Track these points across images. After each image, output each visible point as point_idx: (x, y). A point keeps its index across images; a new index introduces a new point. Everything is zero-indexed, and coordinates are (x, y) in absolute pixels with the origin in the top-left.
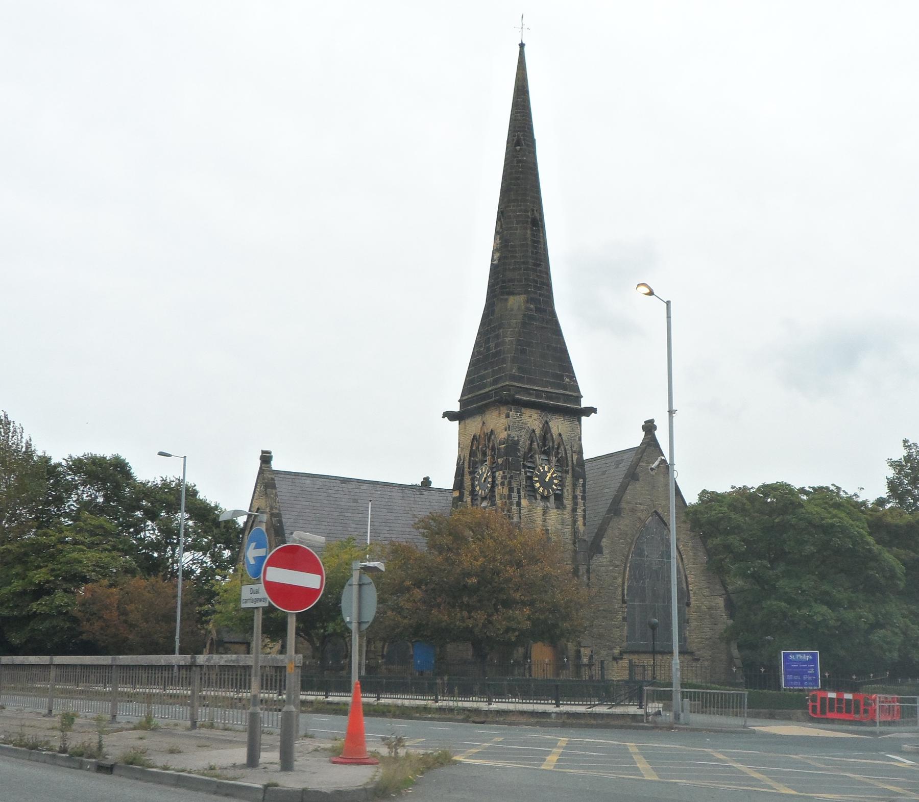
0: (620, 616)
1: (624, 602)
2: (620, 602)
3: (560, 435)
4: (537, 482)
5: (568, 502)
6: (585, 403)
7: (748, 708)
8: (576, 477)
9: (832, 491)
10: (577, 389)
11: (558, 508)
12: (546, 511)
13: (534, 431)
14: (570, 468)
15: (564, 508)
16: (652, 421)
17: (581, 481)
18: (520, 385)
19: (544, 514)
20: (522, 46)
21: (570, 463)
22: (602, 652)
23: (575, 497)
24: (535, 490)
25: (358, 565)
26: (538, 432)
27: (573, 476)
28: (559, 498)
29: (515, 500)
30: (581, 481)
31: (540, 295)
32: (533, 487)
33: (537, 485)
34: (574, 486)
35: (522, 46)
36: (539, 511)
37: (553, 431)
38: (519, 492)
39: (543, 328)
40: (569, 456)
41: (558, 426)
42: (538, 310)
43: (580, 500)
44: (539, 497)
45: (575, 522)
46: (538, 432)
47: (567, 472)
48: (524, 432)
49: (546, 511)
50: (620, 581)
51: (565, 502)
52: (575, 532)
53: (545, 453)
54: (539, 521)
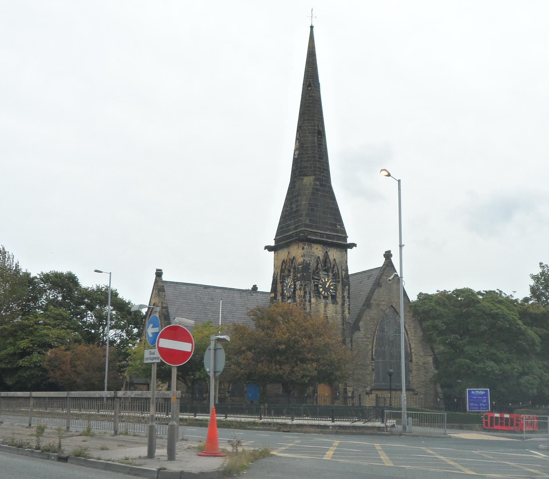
0: (370, 368)
1: (373, 359)
2: (371, 359)
3: (335, 260)
4: (321, 288)
5: (339, 300)
6: (349, 241)
7: (447, 423)
8: (344, 285)
10: (345, 232)
11: (333, 303)
12: (326, 305)
13: (319, 257)
14: (340, 279)
15: (337, 303)
16: (389, 252)
17: (347, 287)
18: (310, 230)
19: (325, 307)
20: (312, 27)
21: (340, 277)
22: (360, 389)
23: (343, 297)
24: (319, 293)
26: (321, 258)
27: (342, 284)
28: (334, 297)
29: (308, 299)
30: (347, 287)
31: (323, 176)
32: (318, 291)
33: (321, 290)
34: (343, 290)
35: (312, 27)
36: (322, 305)
37: (330, 257)
38: (310, 294)
39: (324, 196)
40: (340, 272)
41: (334, 254)
42: (321, 185)
43: (346, 299)
44: (322, 297)
45: (343, 312)
46: (321, 258)
47: (339, 282)
48: (313, 258)
49: (326, 305)
50: (370, 347)
51: (338, 300)
52: (343, 318)
53: (325, 270)
54: (322, 311)
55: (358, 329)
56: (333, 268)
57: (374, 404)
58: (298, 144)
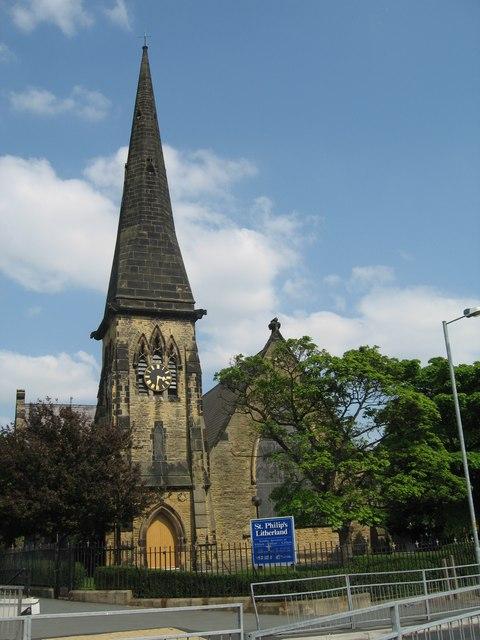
0: (249, 497)
1: (253, 483)
2: (249, 483)
3: (172, 337)
4: (148, 379)
5: (182, 396)
6: (197, 307)
7: (422, 580)
8: (188, 373)
9: (291, 384)
10: (191, 296)
11: (172, 401)
12: (158, 404)
13: (143, 335)
14: (183, 364)
15: (179, 400)
16: (275, 320)
17: (194, 375)
18: (129, 297)
19: (157, 407)
20: (145, 48)
21: (183, 361)
22: (231, 531)
23: (188, 390)
24: (147, 388)
25: (252, 585)
26: (148, 336)
27: (186, 372)
28: (173, 392)
29: (123, 396)
30: (194, 375)
31: (154, 223)
32: (144, 383)
33: (149, 382)
34: (187, 380)
35: (145, 48)
36: (152, 406)
37: (164, 334)
38: (127, 388)
39: (155, 249)
40: (182, 354)
41: (171, 329)
42: (150, 235)
43: (193, 392)
44: (151, 393)
45: (188, 412)
46: (148, 336)
47: (181, 368)
48: (133, 337)
49: (158, 404)
50: (248, 463)
51: (180, 395)
52: (189, 423)
53: (157, 353)
54: (152, 415)
55: (223, 436)
56: (172, 348)
57: (337, 535)
58: (73, 178)
